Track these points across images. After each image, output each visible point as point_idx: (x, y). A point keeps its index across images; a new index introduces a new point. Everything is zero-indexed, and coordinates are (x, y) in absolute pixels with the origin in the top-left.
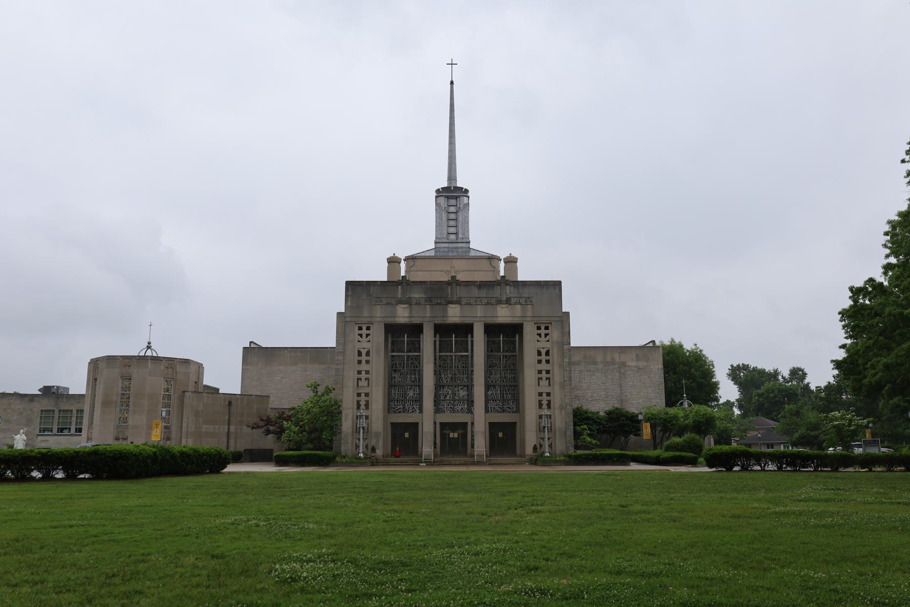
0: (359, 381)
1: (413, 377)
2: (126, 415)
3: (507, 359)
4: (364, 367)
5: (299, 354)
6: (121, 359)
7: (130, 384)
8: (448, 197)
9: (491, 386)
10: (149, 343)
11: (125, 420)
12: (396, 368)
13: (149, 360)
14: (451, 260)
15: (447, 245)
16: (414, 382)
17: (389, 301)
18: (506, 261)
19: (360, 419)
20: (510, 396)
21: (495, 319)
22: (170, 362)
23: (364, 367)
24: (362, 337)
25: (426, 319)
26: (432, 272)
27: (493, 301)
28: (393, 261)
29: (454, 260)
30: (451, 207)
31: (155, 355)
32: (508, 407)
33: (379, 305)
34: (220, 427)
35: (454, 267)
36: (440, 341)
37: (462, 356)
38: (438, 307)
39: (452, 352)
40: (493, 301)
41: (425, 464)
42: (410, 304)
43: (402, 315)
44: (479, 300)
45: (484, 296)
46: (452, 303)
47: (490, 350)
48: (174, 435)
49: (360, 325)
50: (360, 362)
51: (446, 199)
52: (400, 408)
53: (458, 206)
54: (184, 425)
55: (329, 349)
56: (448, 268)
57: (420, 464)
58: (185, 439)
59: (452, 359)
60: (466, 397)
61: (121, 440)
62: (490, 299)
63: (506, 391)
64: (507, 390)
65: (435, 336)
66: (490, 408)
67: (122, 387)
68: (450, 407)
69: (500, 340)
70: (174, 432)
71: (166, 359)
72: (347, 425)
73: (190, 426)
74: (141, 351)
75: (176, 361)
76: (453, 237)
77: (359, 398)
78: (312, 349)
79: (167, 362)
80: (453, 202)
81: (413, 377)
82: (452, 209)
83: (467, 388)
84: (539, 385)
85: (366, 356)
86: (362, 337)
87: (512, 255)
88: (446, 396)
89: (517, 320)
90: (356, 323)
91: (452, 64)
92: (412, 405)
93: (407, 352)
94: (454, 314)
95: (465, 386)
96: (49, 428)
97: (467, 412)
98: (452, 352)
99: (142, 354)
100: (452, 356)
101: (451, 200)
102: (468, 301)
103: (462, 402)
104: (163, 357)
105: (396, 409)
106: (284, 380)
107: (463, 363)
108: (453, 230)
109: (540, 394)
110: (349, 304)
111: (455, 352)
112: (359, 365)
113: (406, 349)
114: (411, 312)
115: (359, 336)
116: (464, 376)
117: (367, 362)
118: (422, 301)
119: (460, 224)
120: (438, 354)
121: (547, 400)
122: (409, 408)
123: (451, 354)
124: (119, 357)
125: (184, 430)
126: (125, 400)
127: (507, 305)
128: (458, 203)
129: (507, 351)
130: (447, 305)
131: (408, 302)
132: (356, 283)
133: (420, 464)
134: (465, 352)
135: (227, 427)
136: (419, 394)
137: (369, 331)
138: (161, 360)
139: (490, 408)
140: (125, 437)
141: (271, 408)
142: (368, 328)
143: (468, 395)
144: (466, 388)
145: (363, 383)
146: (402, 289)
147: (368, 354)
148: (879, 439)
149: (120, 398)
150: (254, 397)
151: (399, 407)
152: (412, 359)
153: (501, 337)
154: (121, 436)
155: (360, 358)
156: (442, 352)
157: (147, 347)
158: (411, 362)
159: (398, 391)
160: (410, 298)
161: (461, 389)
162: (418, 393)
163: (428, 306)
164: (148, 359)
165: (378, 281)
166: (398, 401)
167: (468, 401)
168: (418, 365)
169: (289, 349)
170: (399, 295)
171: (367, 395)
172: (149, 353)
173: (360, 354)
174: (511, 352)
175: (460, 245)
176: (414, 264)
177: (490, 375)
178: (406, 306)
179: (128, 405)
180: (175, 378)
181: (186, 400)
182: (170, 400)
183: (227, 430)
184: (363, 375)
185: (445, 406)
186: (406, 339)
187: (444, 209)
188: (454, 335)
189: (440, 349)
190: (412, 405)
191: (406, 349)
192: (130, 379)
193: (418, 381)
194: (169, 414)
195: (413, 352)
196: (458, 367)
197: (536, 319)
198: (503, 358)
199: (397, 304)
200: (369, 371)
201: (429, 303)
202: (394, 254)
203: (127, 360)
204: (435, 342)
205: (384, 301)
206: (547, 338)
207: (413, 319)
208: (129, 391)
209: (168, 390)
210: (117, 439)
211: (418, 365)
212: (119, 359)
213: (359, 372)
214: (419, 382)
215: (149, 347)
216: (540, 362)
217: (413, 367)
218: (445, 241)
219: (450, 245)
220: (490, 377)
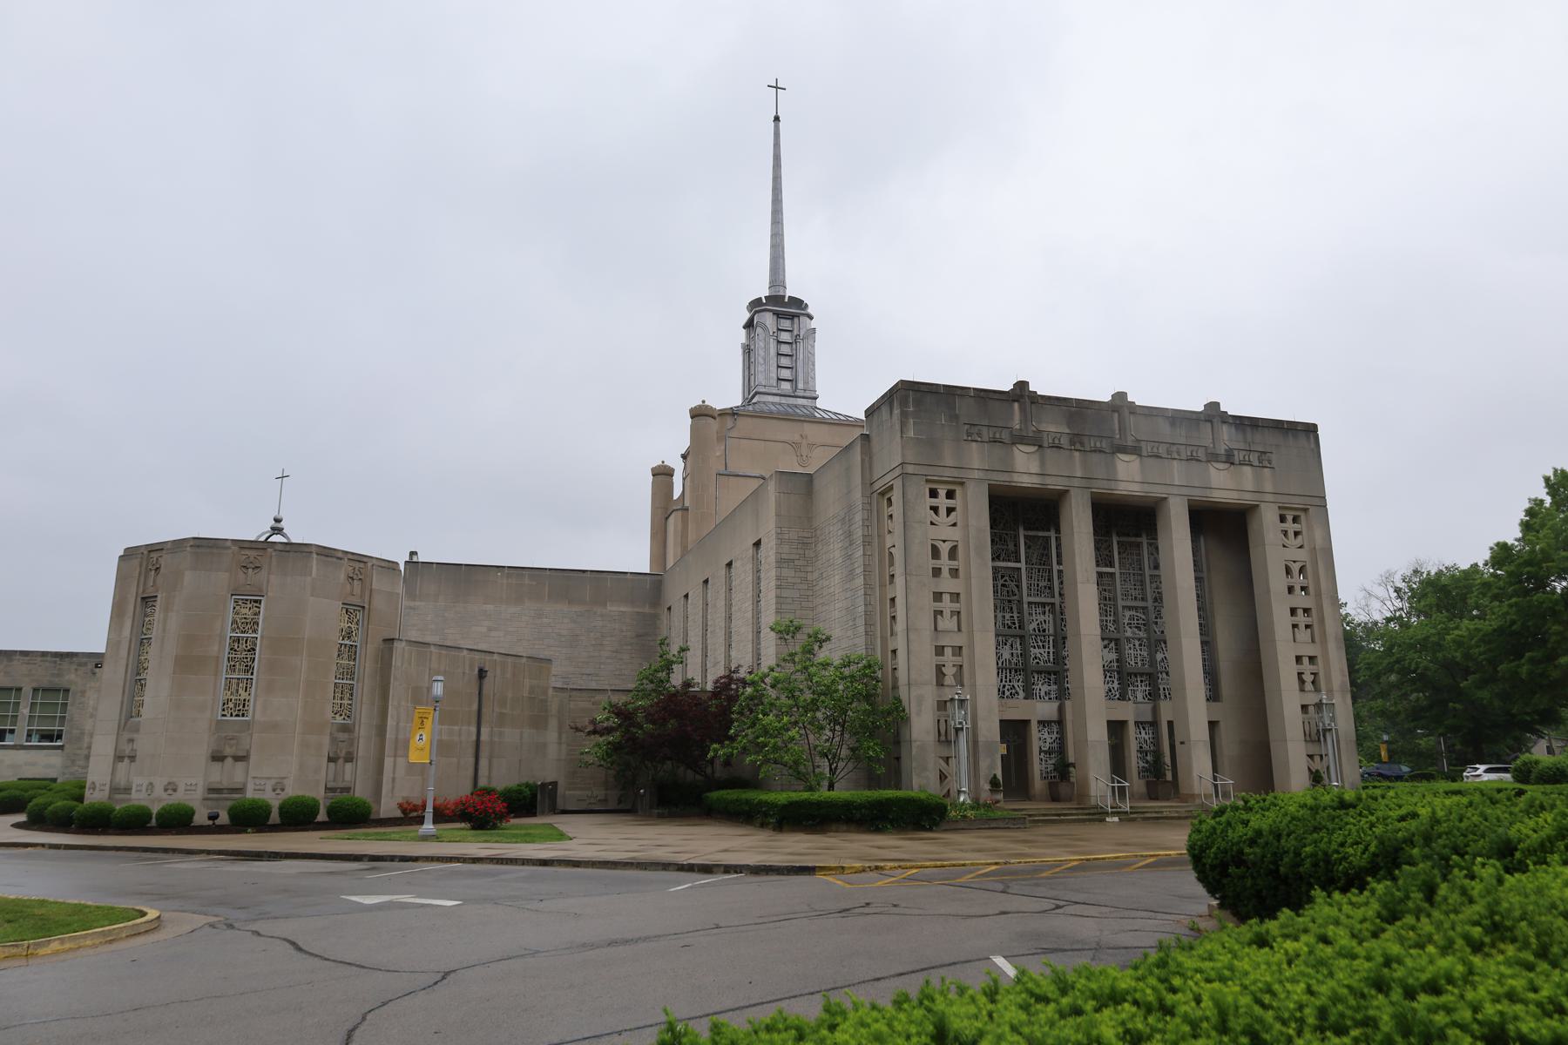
0: (939, 617)
1: (1008, 616)
2: (244, 695)
5: (527, 581)
6: (235, 548)
7: (257, 614)
8: (778, 315)
9: (1159, 641)
10: (278, 520)
11: (241, 708)
13: (315, 556)
14: (799, 424)
15: (777, 399)
16: (1009, 627)
17: (998, 436)
18: (656, 472)
21: (1208, 493)
22: (357, 565)
23: (947, 584)
25: (1076, 483)
26: (768, 443)
27: (1201, 454)
29: (805, 424)
30: (783, 333)
33: (977, 441)
34: (460, 730)
35: (806, 437)
38: (1096, 457)
40: (1201, 454)
41: (1116, 819)
42: (1040, 446)
43: (1026, 469)
44: (1174, 448)
45: (1183, 441)
46: (1123, 450)
47: (1152, 567)
48: (364, 748)
49: (934, 486)
51: (775, 317)
53: (795, 333)
54: (390, 722)
55: (588, 575)
56: (797, 438)
57: (1108, 819)
58: (392, 759)
60: (1116, 664)
61: (229, 760)
62: (1195, 448)
66: (1162, 689)
67: (234, 622)
70: (361, 741)
71: (350, 557)
72: (922, 725)
73: (401, 724)
75: (369, 564)
76: (786, 386)
78: (553, 573)
79: (352, 563)
80: (786, 324)
81: (1008, 616)
82: (785, 337)
83: (1116, 645)
85: (950, 559)
89: (1247, 499)
90: (927, 481)
91: (777, 88)
92: (1010, 681)
95: (1111, 640)
96: (54, 730)
97: (1119, 699)
101: (782, 320)
102: (1155, 450)
103: (1108, 674)
104: (343, 551)
106: (493, 634)
107: (1105, 590)
108: (786, 374)
110: (911, 434)
112: (936, 579)
114: (1042, 463)
115: (932, 512)
116: (1108, 618)
118: (1064, 441)
119: (800, 364)
121: (1312, 674)
122: (1004, 686)
124: (229, 544)
125: (390, 735)
126: (243, 656)
127: (1227, 465)
128: (796, 326)
130: (1113, 453)
131: (1037, 441)
132: (923, 388)
133: (1108, 819)
134: (1106, 566)
135: (474, 729)
136: (1021, 654)
138: (341, 559)
139: (1162, 689)
140: (241, 754)
141: (555, 688)
142: (950, 495)
143: (1118, 661)
144: (1113, 644)
145: (947, 623)
146: (1023, 410)
149: (227, 650)
150: (524, 660)
152: (1002, 577)
154: (228, 751)
157: (273, 528)
158: (1002, 582)
160: (1040, 431)
162: (1019, 652)
163: (1077, 454)
164: (311, 552)
165: (970, 388)
167: (1118, 673)
168: (1016, 590)
169: (506, 571)
170: (1016, 423)
172: (276, 538)
173: (936, 553)
175: (800, 401)
177: (1156, 618)
178: (1032, 449)
179: (249, 669)
180: (367, 606)
181: (397, 661)
182: (355, 659)
183: (474, 738)
184: (947, 605)
187: (771, 334)
188: (588, 587)
192: (256, 601)
193: (1017, 625)
194: (351, 695)
197: (1280, 499)
199: (1013, 444)
201: (1078, 446)
202: (704, 402)
203: (252, 553)
205: (986, 436)
206: (950, 518)
207: (1049, 480)
208: (255, 631)
209: (349, 635)
210: (217, 758)
211: (1016, 590)
212: (229, 548)
213: (938, 596)
214: (1020, 627)
215: (277, 530)
217: (1005, 593)
218: (774, 392)
219: (784, 400)
220: (1156, 623)
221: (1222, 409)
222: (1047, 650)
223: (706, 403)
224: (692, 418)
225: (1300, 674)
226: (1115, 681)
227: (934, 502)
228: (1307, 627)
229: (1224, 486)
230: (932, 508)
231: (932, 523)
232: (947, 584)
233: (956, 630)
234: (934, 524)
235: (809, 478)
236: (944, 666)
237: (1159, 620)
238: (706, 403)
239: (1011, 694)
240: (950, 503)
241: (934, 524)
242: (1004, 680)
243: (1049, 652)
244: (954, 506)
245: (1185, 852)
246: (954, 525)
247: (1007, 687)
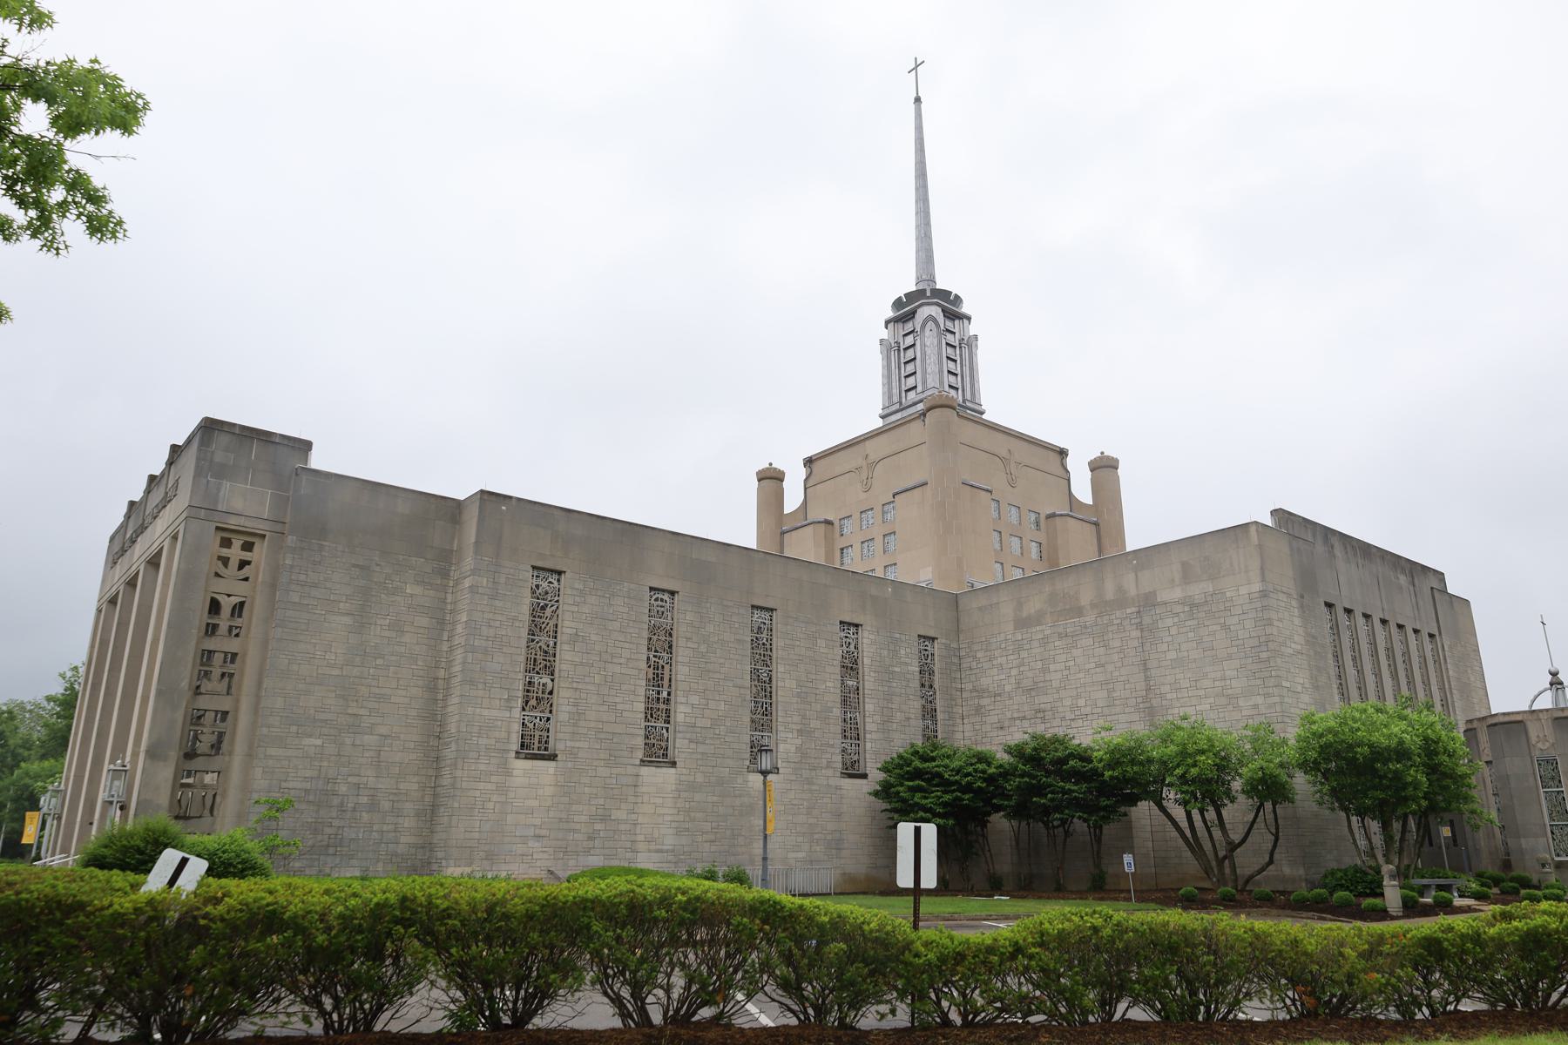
4: (220, 643)
10: (1554, 674)
173: (215, 607)
202: (771, 464)
223: (773, 466)
224: (759, 480)
231: (217, 575)
232: (220, 643)
233: (225, 692)
234: (221, 577)
235: (956, 598)
238: (773, 466)
240: (246, 556)
241: (221, 577)
244: (249, 559)
245: (128, 828)
246: (246, 579)
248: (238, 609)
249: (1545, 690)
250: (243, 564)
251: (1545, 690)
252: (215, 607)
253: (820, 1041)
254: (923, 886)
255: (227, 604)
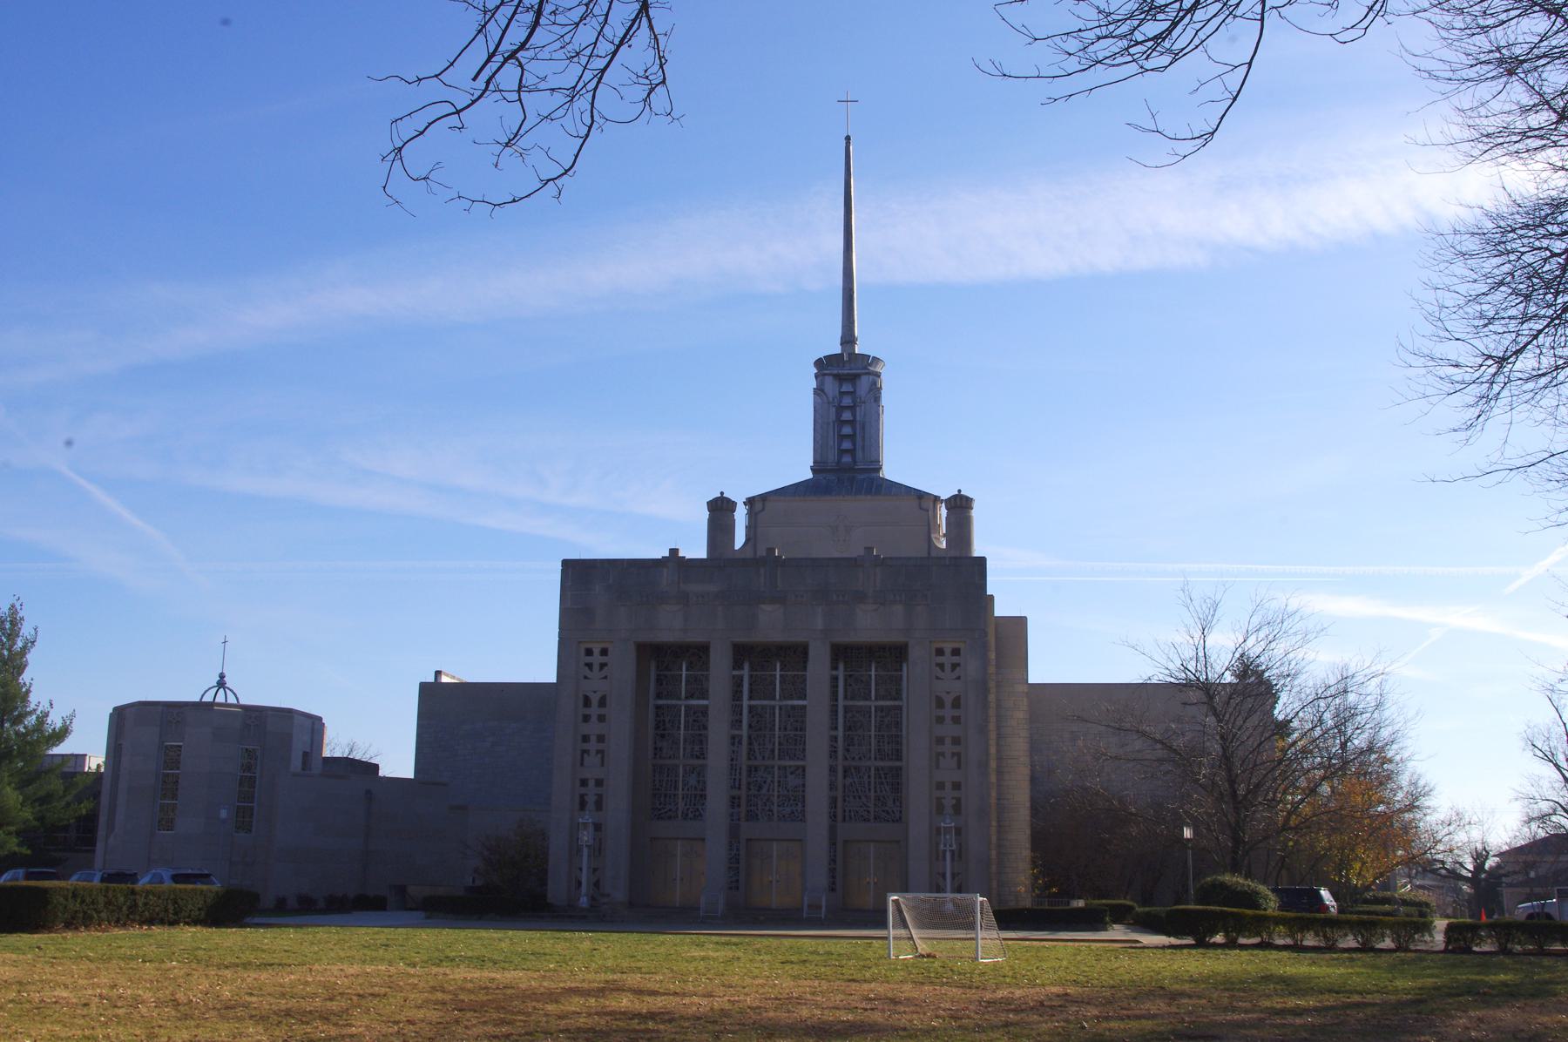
0: (586, 756)
3: (884, 714)
4: (593, 728)
10: (222, 676)
12: (664, 730)
19: (945, 834)
20: (888, 789)
24: (591, 669)
28: (720, 509)
31: (231, 700)
32: (883, 811)
36: (751, 676)
37: (793, 707)
39: (774, 698)
50: (586, 718)
52: (670, 810)
59: (774, 714)
63: (880, 778)
64: (883, 776)
65: (835, 668)
67: (165, 762)
68: (767, 808)
69: (870, 676)
74: (205, 692)
76: (847, 459)
77: (583, 790)
84: (582, 764)
86: (591, 669)
87: (724, 495)
88: (760, 788)
92: (695, 805)
93: (687, 698)
94: (771, 625)
98: (774, 698)
99: (208, 698)
100: (773, 708)
105: (663, 811)
107: (797, 721)
109: (941, 786)
111: (780, 699)
113: (683, 693)
115: (587, 668)
117: (601, 718)
120: (841, 703)
121: (596, 795)
122: (688, 809)
123: (773, 703)
129: (884, 698)
137: (605, 657)
145: (592, 759)
147: (602, 702)
148: (1556, 888)
151: (668, 807)
152: (694, 713)
153: (873, 669)
155: (587, 711)
156: (754, 700)
159: (668, 776)
161: (792, 773)
166: (666, 796)
171: (599, 783)
174: (891, 699)
176: (763, 510)
185: (760, 808)
186: (684, 673)
189: (751, 691)
190: (695, 805)
191: (683, 693)
195: (698, 699)
196: (785, 729)
198: (876, 711)
200: (959, 738)
202: (722, 493)
204: (835, 679)
206: (603, 672)
215: (221, 684)
216: (940, 720)
221: (681, 554)
222: (733, 777)
225: (582, 796)
226: (799, 804)
227: (589, 659)
228: (598, 752)
229: (869, 626)
230: (937, 665)
231: (586, 678)
232: (593, 728)
234: (940, 679)
236: (944, 798)
237: (851, 747)
239: (695, 815)
241: (940, 679)
242: (688, 803)
243: (735, 779)
247: (691, 810)
248: (956, 703)
249: (237, 699)
250: (955, 666)
251: (237, 699)
252: (587, 701)
253: (1566, 336)
254: (217, 700)
255: (948, 700)
